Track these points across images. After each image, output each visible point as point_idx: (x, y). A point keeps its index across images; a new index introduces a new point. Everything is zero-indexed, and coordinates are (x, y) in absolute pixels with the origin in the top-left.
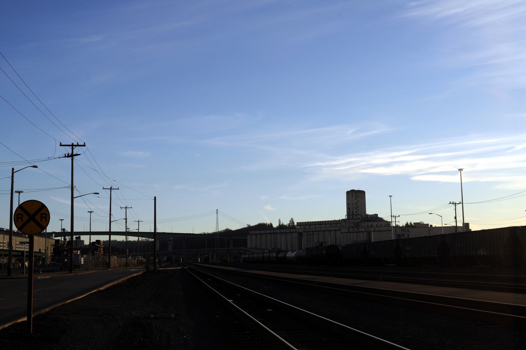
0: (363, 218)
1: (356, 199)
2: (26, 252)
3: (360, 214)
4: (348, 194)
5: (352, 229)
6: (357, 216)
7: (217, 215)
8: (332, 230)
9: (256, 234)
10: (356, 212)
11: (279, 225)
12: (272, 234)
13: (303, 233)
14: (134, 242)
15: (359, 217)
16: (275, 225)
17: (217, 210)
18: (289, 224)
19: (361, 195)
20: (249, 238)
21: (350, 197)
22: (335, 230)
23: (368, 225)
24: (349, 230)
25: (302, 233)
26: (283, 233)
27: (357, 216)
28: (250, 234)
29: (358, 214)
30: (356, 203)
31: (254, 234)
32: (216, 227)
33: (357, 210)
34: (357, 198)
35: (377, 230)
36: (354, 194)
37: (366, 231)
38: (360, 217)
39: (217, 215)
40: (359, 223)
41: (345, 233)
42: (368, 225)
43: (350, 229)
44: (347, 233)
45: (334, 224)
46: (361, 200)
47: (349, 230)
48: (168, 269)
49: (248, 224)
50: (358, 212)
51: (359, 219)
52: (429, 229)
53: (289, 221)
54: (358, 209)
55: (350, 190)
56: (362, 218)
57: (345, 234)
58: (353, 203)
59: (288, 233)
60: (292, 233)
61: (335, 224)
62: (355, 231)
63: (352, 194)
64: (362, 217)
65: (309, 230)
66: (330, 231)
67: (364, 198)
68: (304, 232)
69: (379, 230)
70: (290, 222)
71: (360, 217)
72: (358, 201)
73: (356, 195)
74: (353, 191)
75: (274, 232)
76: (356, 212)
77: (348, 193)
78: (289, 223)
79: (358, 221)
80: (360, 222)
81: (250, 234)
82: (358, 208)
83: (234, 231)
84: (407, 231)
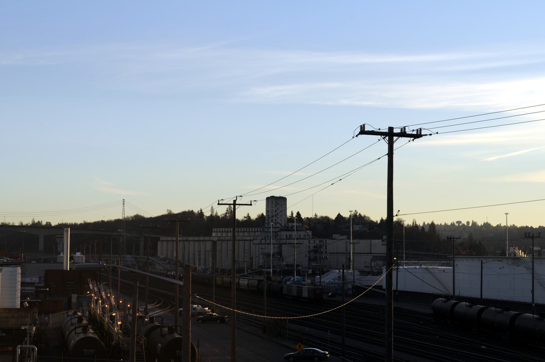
0: (282, 226)
1: (276, 206)
2: (23, 274)
3: (279, 223)
4: (268, 200)
5: (264, 241)
6: (276, 225)
7: (124, 206)
8: (247, 240)
9: (168, 241)
10: (276, 220)
11: (211, 215)
12: (185, 241)
13: (217, 241)
14: (189, 329)
15: (278, 225)
16: (207, 214)
17: (124, 200)
18: (226, 213)
19: (281, 202)
20: (159, 244)
21: (270, 204)
22: (250, 240)
23: (287, 235)
24: (261, 242)
25: (216, 241)
26: (196, 241)
27: (276, 225)
28: (161, 241)
29: (278, 223)
30: (276, 210)
31: (165, 241)
32: (123, 215)
33: (276, 218)
34: (277, 205)
35: (288, 243)
36: (274, 201)
37: (277, 243)
38: (279, 226)
39: (124, 206)
40: (277, 232)
41: (257, 244)
42: (287, 235)
43: (262, 240)
44: (259, 244)
45: (247, 232)
46: (281, 207)
47: (261, 242)
48: (173, 309)
49: (169, 209)
50: (277, 220)
51: (278, 228)
52: (346, 242)
53: (226, 209)
54: (277, 218)
55: (271, 196)
56: (282, 228)
57: (257, 246)
58: (273, 210)
59: (201, 242)
60: (206, 241)
61: (248, 232)
62: (267, 243)
63: (272, 201)
64: (281, 226)
65: (224, 239)
66: (245, 240)
67: (285, 205)
68: (218, 240)
69: (290, 243)
70: (227, 210)
71: (279, 226)
72: (278, 208)
73: (276, 202)
74: (272, 198)
75: (187, 239)
76: (276, 220)
77: (268, 199)
78: (225, 212)
79: (277, 230)
80: (279, 231)
81: (161, 241)
82: (277, 216)
83: (151, 219)
84: (325, 242)
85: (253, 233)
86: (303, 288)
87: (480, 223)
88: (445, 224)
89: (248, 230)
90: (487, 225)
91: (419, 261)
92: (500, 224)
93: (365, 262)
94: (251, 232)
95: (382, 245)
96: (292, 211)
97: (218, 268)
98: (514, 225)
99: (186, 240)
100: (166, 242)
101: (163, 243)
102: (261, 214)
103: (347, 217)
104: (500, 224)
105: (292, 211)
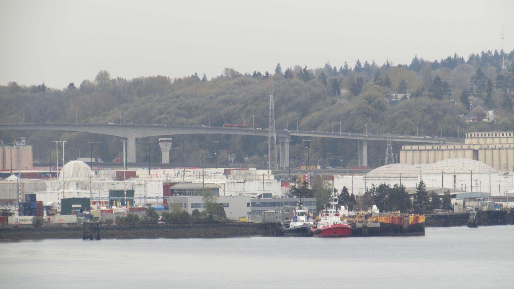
13: (479, 151)
61: (505, 137)
65: (487, 147)
85: (491, 139)
86: (257, 204)
87: (156, 76)
88: (154, 76)
89: (491, 136)
90: (150, 77)
91: (131, 197)
92: (267, 71)
93: (259, 187)
94: (488, 138)
95: (399, 162)
96: (346, 63)
97: (305, 183)
98: (103, 76)
99: (438, 150)
100: (411, 152)
101: (415, 153)
102: (194, 74)
103: (270, 75)
104: (196, 73)
105: (346, 63)
